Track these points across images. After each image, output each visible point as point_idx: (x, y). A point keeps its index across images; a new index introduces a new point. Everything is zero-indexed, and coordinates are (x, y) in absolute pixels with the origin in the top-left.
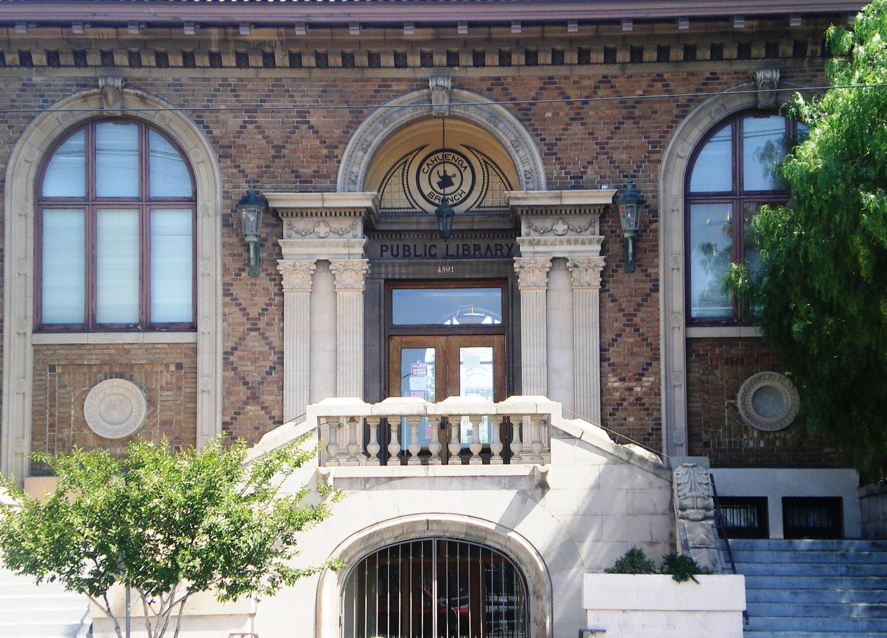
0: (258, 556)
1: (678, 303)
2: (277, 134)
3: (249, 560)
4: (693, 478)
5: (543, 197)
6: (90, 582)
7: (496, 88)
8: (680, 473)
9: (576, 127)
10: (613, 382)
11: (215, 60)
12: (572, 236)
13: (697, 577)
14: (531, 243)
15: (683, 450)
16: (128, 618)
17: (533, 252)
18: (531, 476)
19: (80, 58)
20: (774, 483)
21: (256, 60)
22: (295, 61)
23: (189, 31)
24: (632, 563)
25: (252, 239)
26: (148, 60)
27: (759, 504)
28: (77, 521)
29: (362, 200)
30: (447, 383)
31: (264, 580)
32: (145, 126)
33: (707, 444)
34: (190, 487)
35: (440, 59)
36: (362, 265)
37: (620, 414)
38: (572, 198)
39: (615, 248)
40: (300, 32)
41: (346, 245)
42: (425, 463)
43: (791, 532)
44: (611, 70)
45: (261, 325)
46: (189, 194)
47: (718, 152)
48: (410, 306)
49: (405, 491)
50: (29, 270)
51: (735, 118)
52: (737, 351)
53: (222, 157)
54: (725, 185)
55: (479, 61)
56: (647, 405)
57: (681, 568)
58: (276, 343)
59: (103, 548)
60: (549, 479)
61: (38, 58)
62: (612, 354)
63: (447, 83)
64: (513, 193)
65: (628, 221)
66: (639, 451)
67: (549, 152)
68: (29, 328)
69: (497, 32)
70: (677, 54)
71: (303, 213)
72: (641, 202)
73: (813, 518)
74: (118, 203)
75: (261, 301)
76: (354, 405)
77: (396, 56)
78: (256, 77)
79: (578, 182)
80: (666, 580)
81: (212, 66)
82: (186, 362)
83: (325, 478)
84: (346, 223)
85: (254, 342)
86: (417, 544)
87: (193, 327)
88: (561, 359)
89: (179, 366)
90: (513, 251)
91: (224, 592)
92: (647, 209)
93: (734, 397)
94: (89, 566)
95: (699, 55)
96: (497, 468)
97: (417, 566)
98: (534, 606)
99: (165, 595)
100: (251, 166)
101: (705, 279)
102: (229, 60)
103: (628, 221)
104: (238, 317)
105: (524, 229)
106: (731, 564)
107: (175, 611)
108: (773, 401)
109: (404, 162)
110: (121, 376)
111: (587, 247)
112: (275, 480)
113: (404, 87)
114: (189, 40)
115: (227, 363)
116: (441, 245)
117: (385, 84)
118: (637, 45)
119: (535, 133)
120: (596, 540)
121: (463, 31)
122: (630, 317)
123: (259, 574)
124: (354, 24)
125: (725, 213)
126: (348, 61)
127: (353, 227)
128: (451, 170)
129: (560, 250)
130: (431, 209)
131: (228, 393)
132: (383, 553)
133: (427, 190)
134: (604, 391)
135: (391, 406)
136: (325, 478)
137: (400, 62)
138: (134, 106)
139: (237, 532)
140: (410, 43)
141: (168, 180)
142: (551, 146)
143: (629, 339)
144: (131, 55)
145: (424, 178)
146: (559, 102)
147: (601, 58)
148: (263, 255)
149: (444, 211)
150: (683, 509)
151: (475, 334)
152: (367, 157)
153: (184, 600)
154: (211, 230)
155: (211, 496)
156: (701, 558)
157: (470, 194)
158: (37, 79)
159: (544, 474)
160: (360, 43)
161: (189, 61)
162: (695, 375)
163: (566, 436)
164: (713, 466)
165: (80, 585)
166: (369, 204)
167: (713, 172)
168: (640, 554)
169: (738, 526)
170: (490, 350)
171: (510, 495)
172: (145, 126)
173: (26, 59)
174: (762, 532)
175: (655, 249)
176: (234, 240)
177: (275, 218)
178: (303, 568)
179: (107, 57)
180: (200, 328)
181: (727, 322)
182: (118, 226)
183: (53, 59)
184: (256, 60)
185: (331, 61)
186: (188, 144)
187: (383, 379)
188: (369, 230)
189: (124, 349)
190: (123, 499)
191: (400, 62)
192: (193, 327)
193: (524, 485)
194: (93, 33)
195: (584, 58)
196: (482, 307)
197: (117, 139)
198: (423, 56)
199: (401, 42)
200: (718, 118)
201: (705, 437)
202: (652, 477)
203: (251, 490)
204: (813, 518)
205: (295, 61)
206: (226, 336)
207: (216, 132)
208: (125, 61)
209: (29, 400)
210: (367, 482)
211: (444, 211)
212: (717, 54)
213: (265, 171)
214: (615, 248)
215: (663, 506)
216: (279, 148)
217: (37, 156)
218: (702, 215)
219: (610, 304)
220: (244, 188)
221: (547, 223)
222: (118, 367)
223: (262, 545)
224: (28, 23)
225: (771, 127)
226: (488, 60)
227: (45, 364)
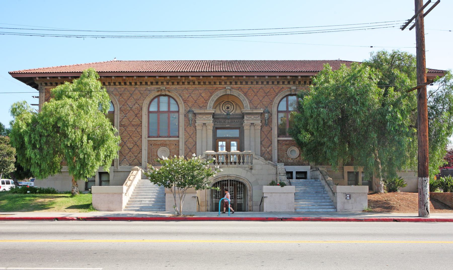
2: (195, 98)
4: (281, 168)
7: (239, 89)
9: (256, 97)
10: (263, 149)
11: (183, 83)
14: (247, 120)
17: (247, 121)
19: (157, 83)
21: (191, 83)
22: (199, 83)
26: (170, 83)
27: (291, 173)
32: (169, 96)
35: (228, 83)
39: (264, 121)
44: (263, 86)
45: (192, 136)
47: (283, 103)
48: (220, 133)
50: (147, 125)
52: (287, 143)
56: (270, 153)
58: (195, 140)
61: (149, 83)
62: (263, 143)
63: (230, 88)
67: (250, 102)
69: (240, 78)
71: (200, 114)
75: (192, 132)
77: (220, 82)
78: (191, 87)
79: (256, 108)
82: (177, 144)
85: (190, 140)
87: (178, 137)
89: (176, 145)
95: (259, 83)
100: (190, 104)
102: (186, 83)
104: (187, 135)
105: (245, 117)
109: (220, 104)
114: (179, 79)
115: (185, 144)
116: (227, 121)
122: (266, 135)
128: (229, 106)
130: (226, 114)
131: (185, 150)
133: (224, 110)
134: (261, 150)
137: (220, 83)
138: (168, 93)
141: (174, 108)
142: (250, 101)
143: (266, 140)
145: (223, 107)
146: (252, 92)
149: (228, 114)
152: (213, 103)
156: (285, 182)
157: (234, 111)
161: (178, 83)
162: (279, 147)
164: (285, 165)
168: (274, 182)
170: (219, 142)
173: (146, 83)
175: (271, 122)
179: (162, 83)
180: (180, 137)
183: (152, 83)
184: (191, 83)
191: (220, 83)
192: (178, 137)
196: (236, 133)
197: (164, 100)
198: (225, 82)
204: (302, 175)
206: (185, 139)
213: (193, 105)
215: (275, 173)
217: (148, 103)
218: (281, 115)
221: (250, 116)
227: (150, 144)
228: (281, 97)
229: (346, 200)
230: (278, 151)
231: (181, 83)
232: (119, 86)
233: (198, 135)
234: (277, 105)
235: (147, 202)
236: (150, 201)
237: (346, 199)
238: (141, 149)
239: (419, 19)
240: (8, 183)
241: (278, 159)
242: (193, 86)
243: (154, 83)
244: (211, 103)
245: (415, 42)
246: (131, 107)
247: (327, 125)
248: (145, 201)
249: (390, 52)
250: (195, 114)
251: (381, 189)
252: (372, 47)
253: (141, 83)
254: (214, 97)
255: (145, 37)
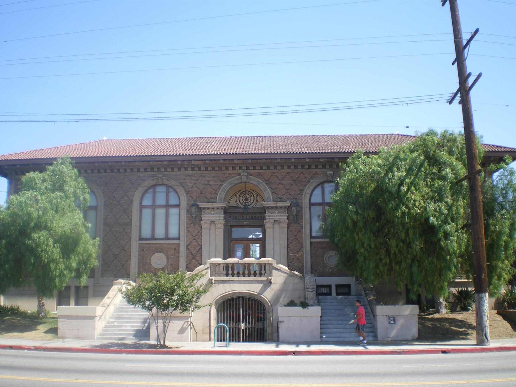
0: (190, 302)
1: (308, 232)
3: (187, 303)
4: (311, 281)
5: (271, 204)
6: (147, 307)
7: (259, 175)
8: (307, 279)
9: (281, 185)
10: (291, 254)
11: (186, 169)
12: (280, 214)
13: (309, 307)
14: (269, 216)
15: (310, 272)
16: (157, 317)
17: (269, 218)
18: (267, 280)
19: (152, 170)
20: (334, 281)
21: (196, 169)
22: (207, 169)
23: (179, 162)
24: (291, 304)
25: (194, 215)
27: (330, 286)
28: (144, 291)
29: (223, 205)
30: (247, 254)
31: (191, 308)
32: (168, 186)
33: (316, 271)
34: (172, 283)
35: (244, 168)
36: (223, 222)
37: (293, 263)
38: (279, 204)
40: (208, 162)
41: (219, 217)
42: (238, 276)
43: (338, 294)
45: (196, 238)
46: (178, 203)
47: (318, 192)
48: (237, 233)
49: (64, 307)
50: (138, 225)
51: (322, 183)
53: (187, 194)
54: (320, 201)
55: (254, 168)
56: (300, 260)
57: (304, 305)
59: (151, 299)
60: (272, 281)
61: (102, 171)
62: (290, 246)
63: (246, 174)
64: (265, 203)
65: (295, 210)
66: (296, 273)
67: (273, 192)
68: (138, 239)
70: (306, 167)
71: (208, 208)
72: (298, 205)
73: (344, 290)
74: (161, 206)
75: (196, 232)
76: (219, 260)
77: (233, 167)
79: (281, 200)
80: (300, 308)
81: (185, 171)
83: (212, 280)
84: (219, 211)
85: (194, 243)
86: (236, 298)
87: (178, 239)
88: (277, 248)
89: (175, 249)
90: (264, 218)
91: (181, 311)
92: (299, 207)
93: (323, 258)
94: (148, 303)
96: (258, 278)
97: (236, 304)
98: (268, 315)
99: (166, 312)
101: (317, 225)
103: (295, 210)
106: (318, 303)
107: (169, 315)
108: (332, 259)
109: (235, 194)
110: (160, 252)
111: (284, 217)
112: (195, 282)
113: (235, 175)
115: (187, 248)
116: (245, 216)
117: (230, 174)
118: (310, 164)
119: (270, 187)
120: (284, 297)
121: (250, 161)
123: (190, 307)
124: (221, 160)
125: (320, 208)
126: (220, 169)
127: (221, 212)
128: (248, 196)
129: (276, 218)
131: (187, 257)
132: (227, 301)
133: (241, 202)
135: (230, 260)
136: (212, 280)
137: (234, 169)
138: (166, 182)
139: (184, 295)
140: (236, 164)
141: (173, 200)
142: (274, 190)
144: (165, 168)
145: (241, 199)
147: (287, 168)
148: (197, 220)
149: (246, 207)
150: (307, 289)
151: (256, 241)
152: (225, 193)
153: (171, 313)
154: (184, 212)
155: (178, 286)
156: (310, 302)
157: (253, 202)
158: (141, 175)
159: (271, 279)
160: (223, 164)
161: (179, 169)
163: (277, 269)
165: (145, 308)
166: (225, 206)
167: (317, 198)
169: (322, 292)
171: (260, 286)
172: (168, 186)
173: (139, 170)
174: (330, 294)
176: (190, 216)
177: (200, 210)
178: (202, 305)
179: (159, 169)
181: (322, 237)
182: (160, 212)
183: (146, 170)
184: (196, 169)
185: (216, 169)
186: (178, 191)
187: (229, 253)
188: (225, 212)
189: (161, 245)
190: (155, 286)
192: (178, 239)
193: (265, 282)
194: (155, 163)
195: (282, 167)
198: (240, 167)
199: (234, 164)
200: (318, 183)
201: (316, 269)
202: (300, 280)
203: (188, 284)
204: (344, 290)
205: (207, 169)
206: (187, 241)
207: (186, 188)
208: (163, 170)
209: (137, 258)
210: (223, 282)
211: (246, 207)
212: (317, 167)
214: (291, 217)
216: (202, 191)
217: (141, 195)
219: (290, 233)
220: (193, 202)
221: (273, 211)
222: (160, 249)
223: (191, 299)
224: (139, 161)
225: (332, 186)
226: (257, 168)
227: (142, 248)
228: (314, 185)
229: (389, 325)
230: (311, 257)
231: (183, 169)
232: (104, 174)
233: (205, 237)
234: (308, 196)
235: (129, 328)
236: (133, 326)
237: (389, 323)
238: (130, 256)
239: (464, 94)
240: (460, 246)
241: (312, 268)
242: (199, 172)
243: (149, 170)
244: (221, 194)
245: (462, 121)
246: (118, 200)
247: (498, 203)
248: (126, 326)
249: (439, 131)
250: (200, 209)
251: (441, 308)
252: (408, 127)
253: (132, 170)
254: (226, 187)
255: (127, 119)
